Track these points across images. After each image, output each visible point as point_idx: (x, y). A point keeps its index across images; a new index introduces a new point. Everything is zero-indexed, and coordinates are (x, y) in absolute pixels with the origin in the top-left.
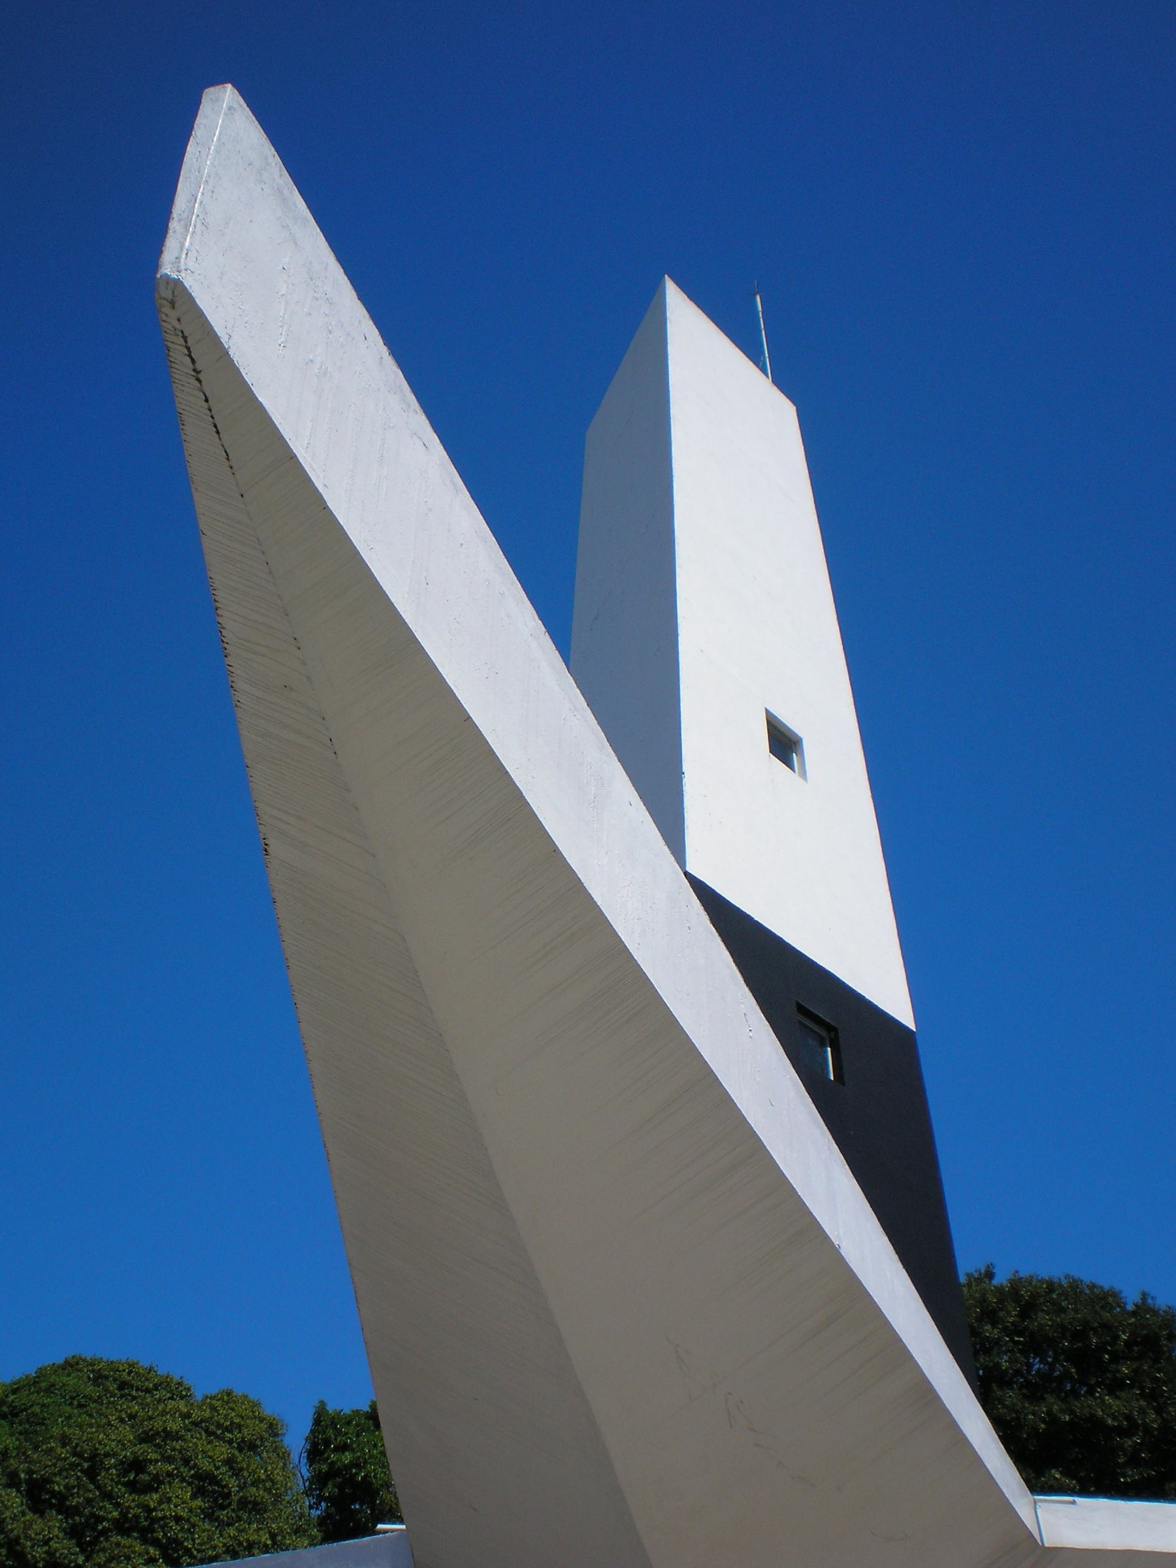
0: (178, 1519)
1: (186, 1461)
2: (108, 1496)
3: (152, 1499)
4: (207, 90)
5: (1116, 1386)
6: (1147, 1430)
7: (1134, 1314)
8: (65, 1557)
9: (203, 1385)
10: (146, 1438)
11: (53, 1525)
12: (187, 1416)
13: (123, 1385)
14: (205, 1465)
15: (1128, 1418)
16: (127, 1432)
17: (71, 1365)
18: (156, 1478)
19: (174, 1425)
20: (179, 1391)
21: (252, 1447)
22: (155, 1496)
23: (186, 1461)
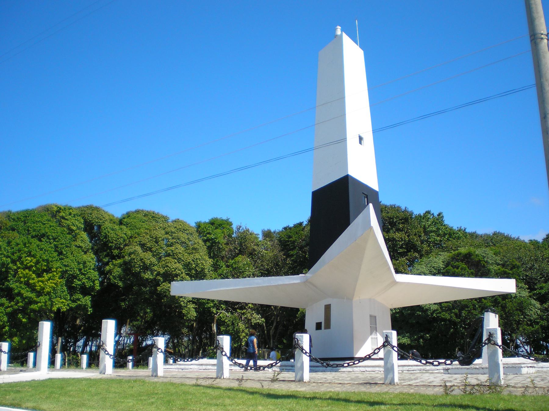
0: (180, 253)
1: (179, 239)
2: (162, 248)
3: (173, 248)
4: (362, 52)
5: (398, 230)
6: (405, 241)
7: (403, 212)
8: (463, 338)
9: (172, 217)
10: (167, 233)
11: (149, 255)
12: (176, 227)
13: (153, 217)
14: (184, 240)
15: (401, 238)
16: (163, 232)
17: (137, 212)
18: (172, 243)
19: (173, 230)
20: (166, 219)
21: (191, 234)
22: (174, 248)
23: (179, 239)
